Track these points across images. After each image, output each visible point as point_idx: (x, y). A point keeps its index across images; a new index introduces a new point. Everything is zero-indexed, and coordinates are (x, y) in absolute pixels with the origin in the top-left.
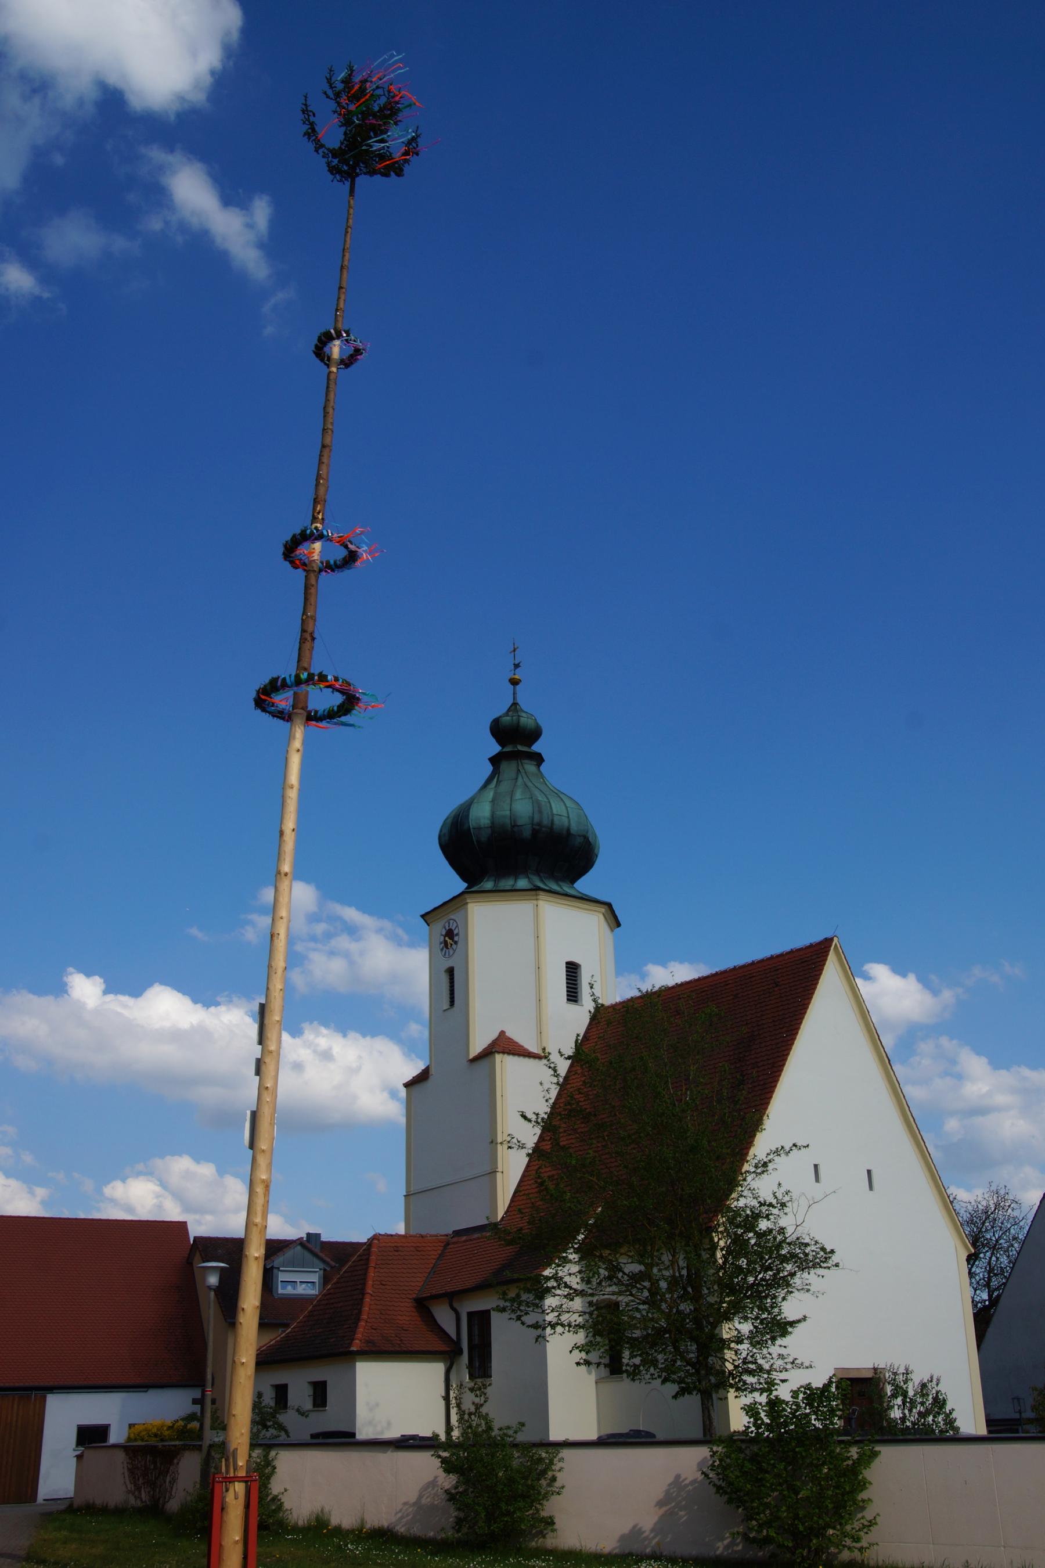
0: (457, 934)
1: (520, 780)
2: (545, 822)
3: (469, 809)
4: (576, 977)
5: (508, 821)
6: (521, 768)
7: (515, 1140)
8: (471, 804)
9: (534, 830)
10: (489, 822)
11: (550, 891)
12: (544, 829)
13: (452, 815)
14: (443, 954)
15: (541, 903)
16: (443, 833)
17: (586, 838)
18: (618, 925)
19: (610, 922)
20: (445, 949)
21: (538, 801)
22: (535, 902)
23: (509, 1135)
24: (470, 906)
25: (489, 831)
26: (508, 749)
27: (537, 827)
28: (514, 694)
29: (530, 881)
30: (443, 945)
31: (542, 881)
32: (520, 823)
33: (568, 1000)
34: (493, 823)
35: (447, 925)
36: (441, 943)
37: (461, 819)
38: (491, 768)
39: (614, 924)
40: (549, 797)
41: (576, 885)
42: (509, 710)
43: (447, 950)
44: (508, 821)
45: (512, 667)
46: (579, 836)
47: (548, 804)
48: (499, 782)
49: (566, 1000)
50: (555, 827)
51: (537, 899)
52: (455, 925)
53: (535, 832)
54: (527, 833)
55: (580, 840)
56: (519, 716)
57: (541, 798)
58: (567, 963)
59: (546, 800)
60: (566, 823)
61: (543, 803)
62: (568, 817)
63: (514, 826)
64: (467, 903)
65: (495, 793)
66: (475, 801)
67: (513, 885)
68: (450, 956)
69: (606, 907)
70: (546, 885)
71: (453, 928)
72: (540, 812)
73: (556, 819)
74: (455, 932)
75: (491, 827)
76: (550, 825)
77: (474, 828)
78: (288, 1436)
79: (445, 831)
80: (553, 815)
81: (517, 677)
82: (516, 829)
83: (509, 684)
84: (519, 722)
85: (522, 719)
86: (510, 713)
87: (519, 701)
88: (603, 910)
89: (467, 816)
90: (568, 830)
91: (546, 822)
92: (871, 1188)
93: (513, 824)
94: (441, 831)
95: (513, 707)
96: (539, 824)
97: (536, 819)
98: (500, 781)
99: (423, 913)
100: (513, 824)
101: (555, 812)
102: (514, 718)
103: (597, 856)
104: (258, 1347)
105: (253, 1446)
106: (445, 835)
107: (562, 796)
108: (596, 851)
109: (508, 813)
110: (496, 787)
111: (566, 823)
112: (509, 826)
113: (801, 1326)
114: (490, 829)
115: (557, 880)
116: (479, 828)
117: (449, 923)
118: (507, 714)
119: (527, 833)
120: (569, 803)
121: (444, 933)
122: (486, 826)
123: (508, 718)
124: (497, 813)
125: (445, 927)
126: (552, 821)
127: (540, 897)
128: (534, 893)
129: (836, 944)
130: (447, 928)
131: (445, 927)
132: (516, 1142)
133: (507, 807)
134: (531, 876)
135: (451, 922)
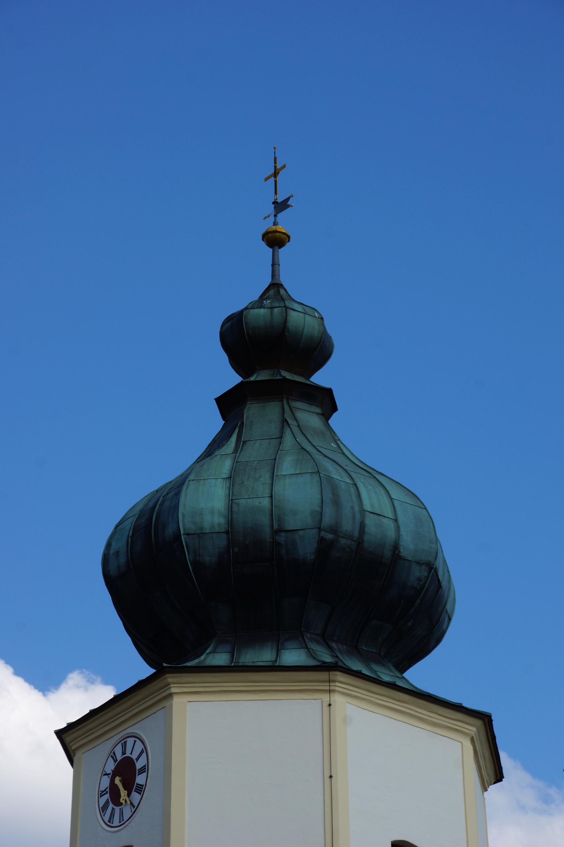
0: (144, 770)
1: (288, 438)
2: (348, 526)
3: (178, 494)
5: (265, 520)
6: (288, 416)
8: (183, 484)
9: (322, 540)
10: (222, 521)
11: (358, 675)
12: (343, 541)
13: (137, 511)
14: (106, 818)
15: (338, 699)
16: (114, 546)
17: (431, 568)
18: (499, 777)
19: (482, 764)
20: (111, 806)
21: (330, 479)
22: (325, 698)
24: (177, 701)
25: (222, 542)
26: (261, 376)
27: (330, 536)
28: (275, 264)
29: (311, 654)
30: (107, 796)
32: (290, 524)
34: (231, 522)
35: (118, 751)
36: (102, 794)
37: (264, 305)
38: (221, 423)
39: (489, 772)
40: (353, 475)
41: (406, 675)
42: (263, 296)
43: (117, 809)
44: (265, 520)
45: (271, 208)
46: (418, 563)
47: (352, 490)
48: (240, 444)
50: (366, 538)
51: (330, 691)
52: (139, 747)
55: (418, 572)
56: (286, 307)
57: (336, 474)
59: (348, 480)
61: (343, 485)
62: (396, 520)
64: (170, 695)
65: (236, 463)
66: (192, 477)
67: (276, 661)
68: (122, 822)
69: (479, 722)
71: (134, 756)
72: (336, 503)
73: (370, 521)
74: (139, 765)
75: (227, 532)
76: (356, 534)
77: (188, 534)
79: (120, 545)
80: (363, 511)
81: (280, 228)
82: (282, 538)
83: (263, 244)
85: (292, 314)
86: (267, 303)
87: (283, 280)
88: (472, 730)
89: (176, 508)
90: (396, 547)
93: (276, 527)
94: (109, 545)
95: (272, 292)
96: (335, 530)
97: (327, 520)
98: (244, 442)
99: (63, 725)
100: (276, 527)
101: (367, 506)
102: (276, 310)
103: (450, 619)
104: (166, 703)
106: (117, 553)
107: (378, 477)
108: (448, 607)
109: (266, 502)
110: (236, 450)
111: (391, 533)
112: (268, 530)
114: (224, 536)
115: (367, 659)
116: (201, 535)
117: (124, 746)
118: (259, 303)
120: (395, 493)
121: (111, 766)
122: (217, 530)
123: (262, 311)
124: (242, 502)
125: (114, 757)
126: (362, 526)
127: (338, 686)
128: (323, 675)
130: (119, 757)
131: (114, 757)
133: (262, 489)
134: (313, 646)
135: (130, 741)
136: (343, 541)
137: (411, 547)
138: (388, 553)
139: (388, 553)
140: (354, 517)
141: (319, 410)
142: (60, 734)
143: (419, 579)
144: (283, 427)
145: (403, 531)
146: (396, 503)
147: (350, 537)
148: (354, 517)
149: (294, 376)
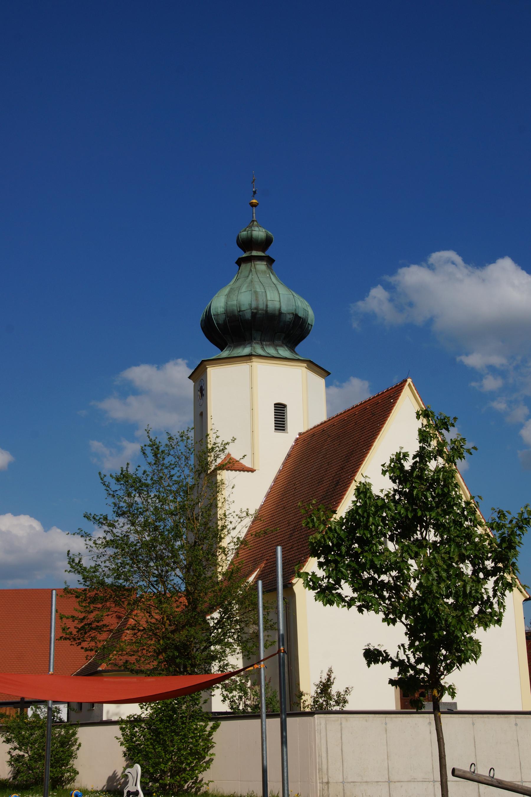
4: (284, 427)
5: (235, 308)
7: (83, 532)
9: (252, 313)
10: (223, 310)
12: (260, 312)
15: (254, 364)
22: (250, 364)
23: (79, 529)
24: (209, 370)
25: (224, 316)
27: (255, 311)
31: (263, 348)
32: (243, 309)
33: (275, 429)
46: (289, 314)
49: (274, 428)
50: (268, 309)
51: (251, 362)
53: (254, 315)
54: (248, 316)
58: (275, 404)
60: (294, 307)
63: (240, 311)
70: (264, 350)
72: (257, 299)
76: (265, 308)
78: (398, 651)
82: (241, 313)
84: (252, 235)
88: (305, 365)
90: (280, 310)
91: (261, 306)
93: (238, 310)
96: (257, 308)
97: (254, 306)
101: (269, 298)
105: (193, 673)
113: (333, 676)
116: (217, 315)
119: (248, 316)
126: (267, 305)
127: (254, 360)
128: (248, 358)
129: (409, 383)
132: (84, 533)
136: (260, 312)
137: (286, 309)
138: (277, 313)
139: (277, 313)
140: (263, 303)
141: (265, 263)
142: (189, 377)
143: (290, 319)
144: (250, 272)
145: (282, 304)
146: (281, 295)
147: (263, 310)
148: (263, 303)
149: (258, 252)
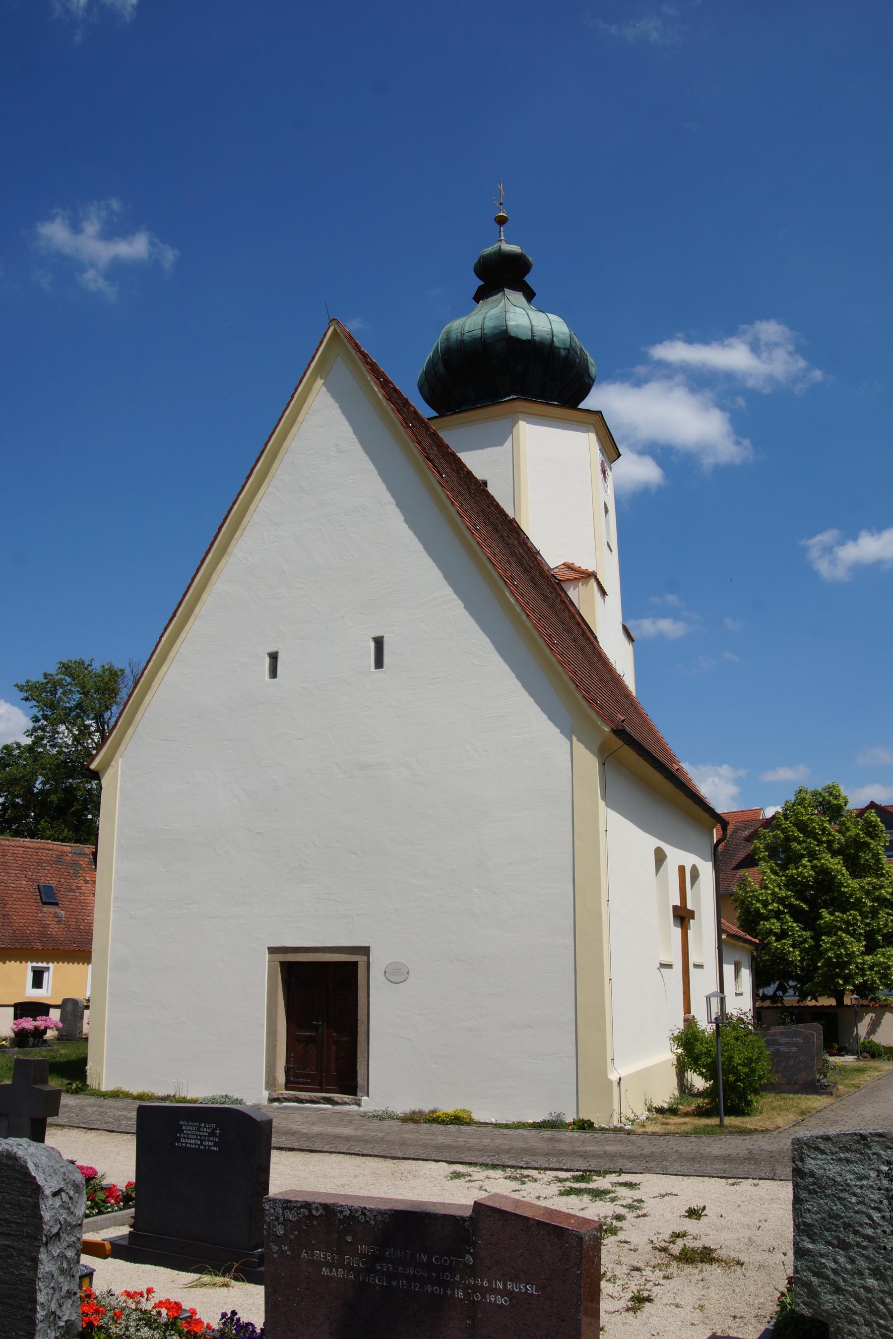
92: (379, 663)
